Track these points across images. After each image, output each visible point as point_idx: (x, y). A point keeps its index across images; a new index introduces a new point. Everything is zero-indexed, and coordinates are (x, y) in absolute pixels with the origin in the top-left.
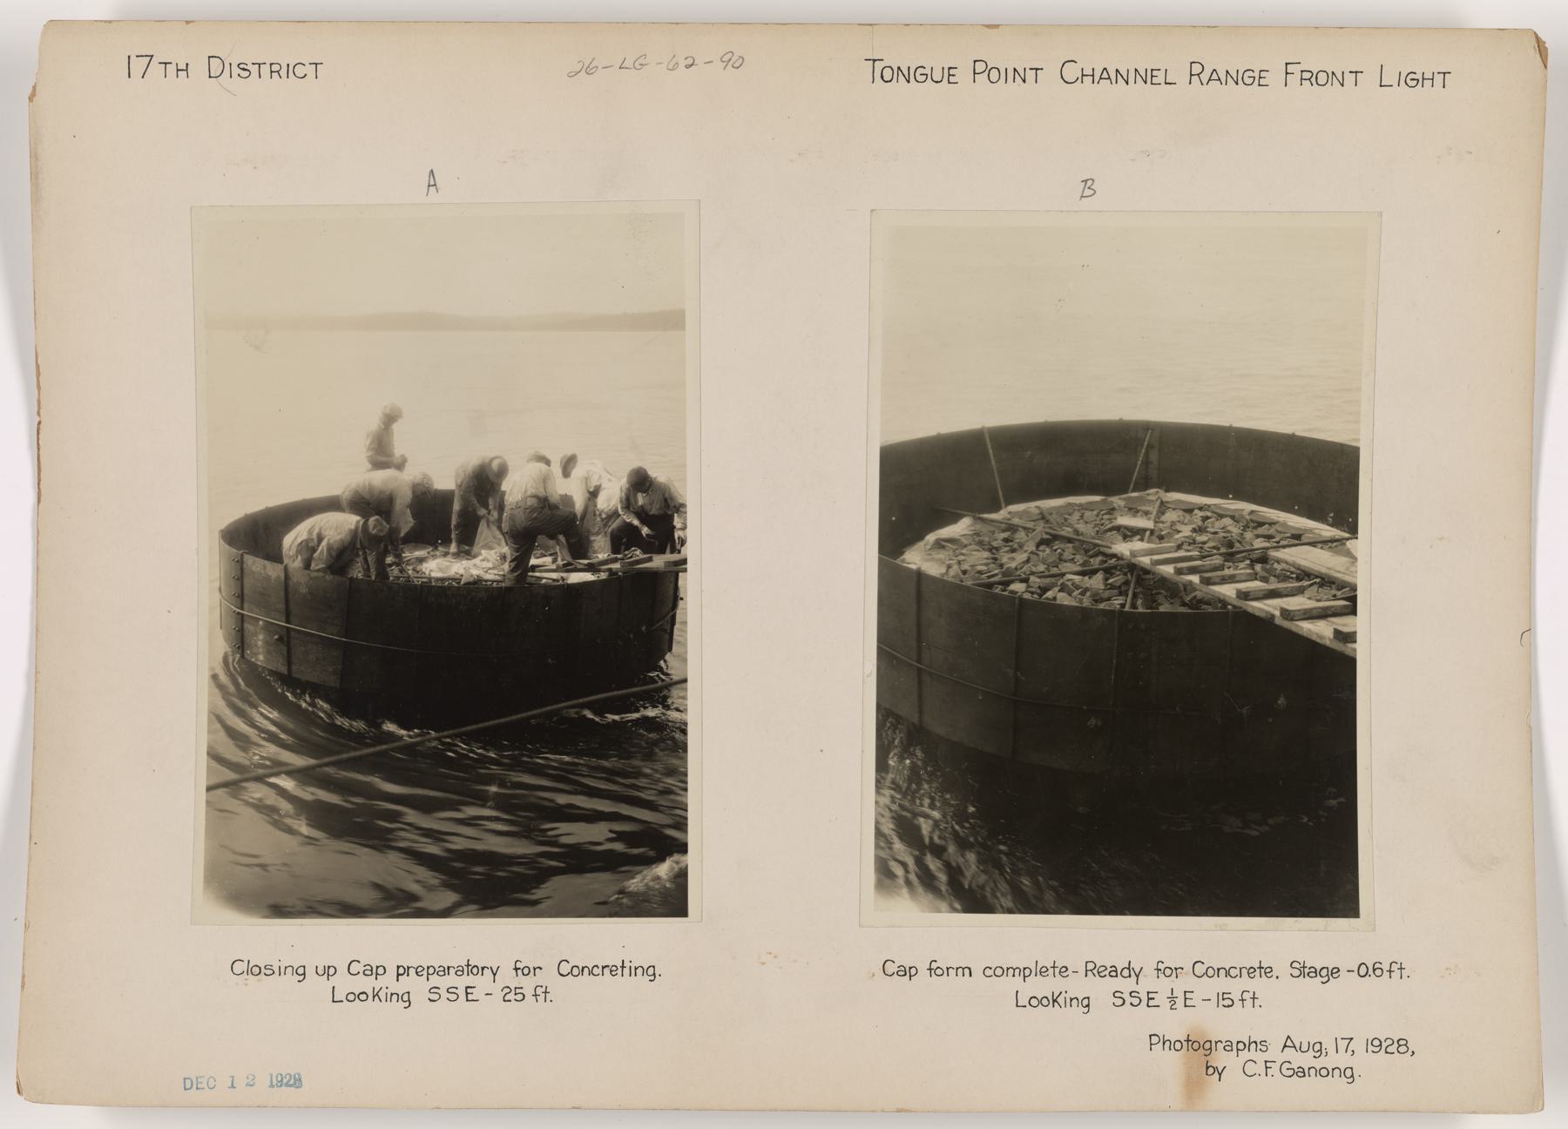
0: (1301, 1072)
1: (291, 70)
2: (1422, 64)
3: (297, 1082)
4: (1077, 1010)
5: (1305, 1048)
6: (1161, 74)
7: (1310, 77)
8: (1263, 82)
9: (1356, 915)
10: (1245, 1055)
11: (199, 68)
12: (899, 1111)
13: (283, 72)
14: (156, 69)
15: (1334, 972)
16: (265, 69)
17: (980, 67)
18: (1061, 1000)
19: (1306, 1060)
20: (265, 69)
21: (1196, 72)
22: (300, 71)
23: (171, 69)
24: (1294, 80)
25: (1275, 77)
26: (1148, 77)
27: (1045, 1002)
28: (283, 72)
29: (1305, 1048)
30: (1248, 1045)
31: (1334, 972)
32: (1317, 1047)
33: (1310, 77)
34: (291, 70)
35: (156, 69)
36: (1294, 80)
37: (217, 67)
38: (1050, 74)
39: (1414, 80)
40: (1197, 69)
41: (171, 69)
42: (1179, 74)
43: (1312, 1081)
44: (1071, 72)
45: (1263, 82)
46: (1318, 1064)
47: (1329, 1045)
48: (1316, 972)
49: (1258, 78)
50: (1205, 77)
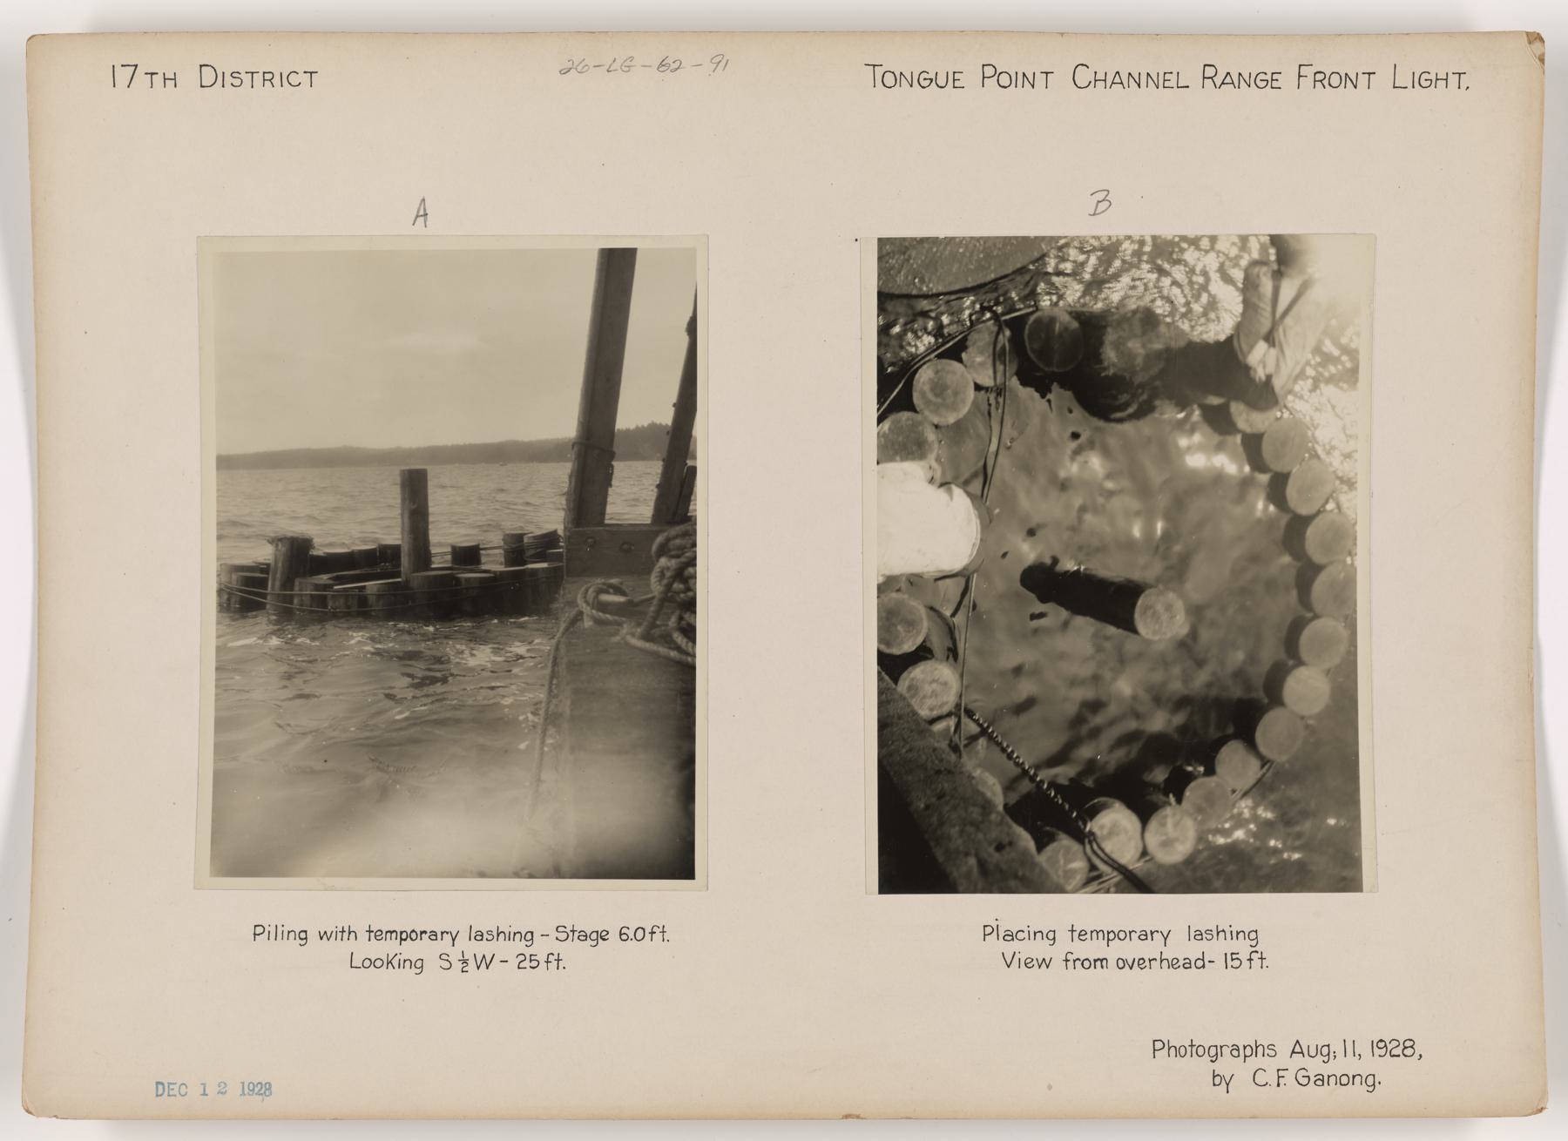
0: (1321, 1080)
1: (286, 79)
2: (1437, 63)
3: (265, 1089)
4: (409, 972)
5: (1313, 1053)
6: (1173, 77)
7: (1321, 79)
8: (1275, 84)
9: (882, 891)
10: (1254, 1062)
11: (189, 77)
12: (847, 1117)
13: (276, 81)
14: (141, 80)
15: (602, 936)
16: (258, 78)
17: (989, 71)
18: (395, 962)
19: (1315, 1066)
20: (258, 78)
21: (1209, 74)
22: (294, 79)
23: (158, 79)
24: (1307, 82)
25: (1288, 79)
26: (1161, 81)
27: (378, 963)
28: (276, 81)
29: (1313, 1053)
30: (1255, 1049)
31: (602, 936)
32: (1325, 1051)
33: (1321, 79)
34: (286, 79)
35: (141, 80)
36: (1307, 82)
37: (214, 77)
38: (1061, 78)
39: (1423, 81)
40: (1210, 72)
41: (158, 79)
42: (1192, 76)
43: (1331, 1089)
44: (1084, 76)
45: (1275, 84)
46: (1326, 1070)
47: (1337, 1047)
48: (584, 936)
49: (1271, 81)
50: (1218, 80)
